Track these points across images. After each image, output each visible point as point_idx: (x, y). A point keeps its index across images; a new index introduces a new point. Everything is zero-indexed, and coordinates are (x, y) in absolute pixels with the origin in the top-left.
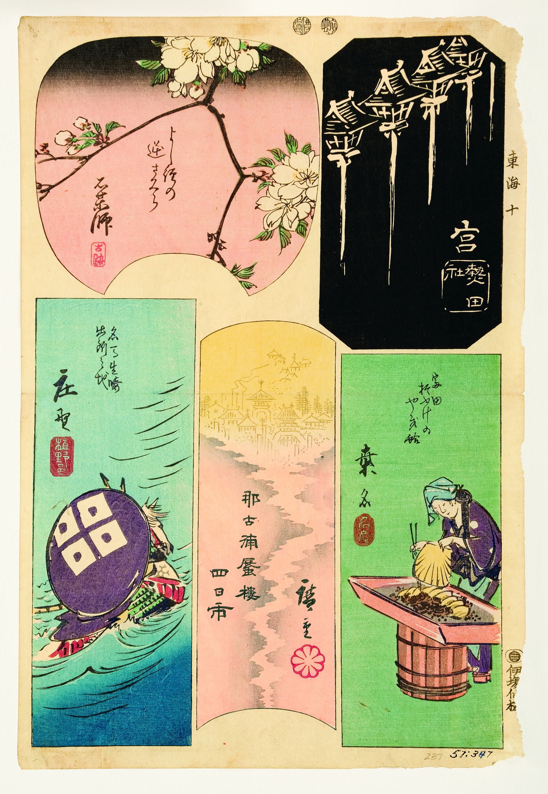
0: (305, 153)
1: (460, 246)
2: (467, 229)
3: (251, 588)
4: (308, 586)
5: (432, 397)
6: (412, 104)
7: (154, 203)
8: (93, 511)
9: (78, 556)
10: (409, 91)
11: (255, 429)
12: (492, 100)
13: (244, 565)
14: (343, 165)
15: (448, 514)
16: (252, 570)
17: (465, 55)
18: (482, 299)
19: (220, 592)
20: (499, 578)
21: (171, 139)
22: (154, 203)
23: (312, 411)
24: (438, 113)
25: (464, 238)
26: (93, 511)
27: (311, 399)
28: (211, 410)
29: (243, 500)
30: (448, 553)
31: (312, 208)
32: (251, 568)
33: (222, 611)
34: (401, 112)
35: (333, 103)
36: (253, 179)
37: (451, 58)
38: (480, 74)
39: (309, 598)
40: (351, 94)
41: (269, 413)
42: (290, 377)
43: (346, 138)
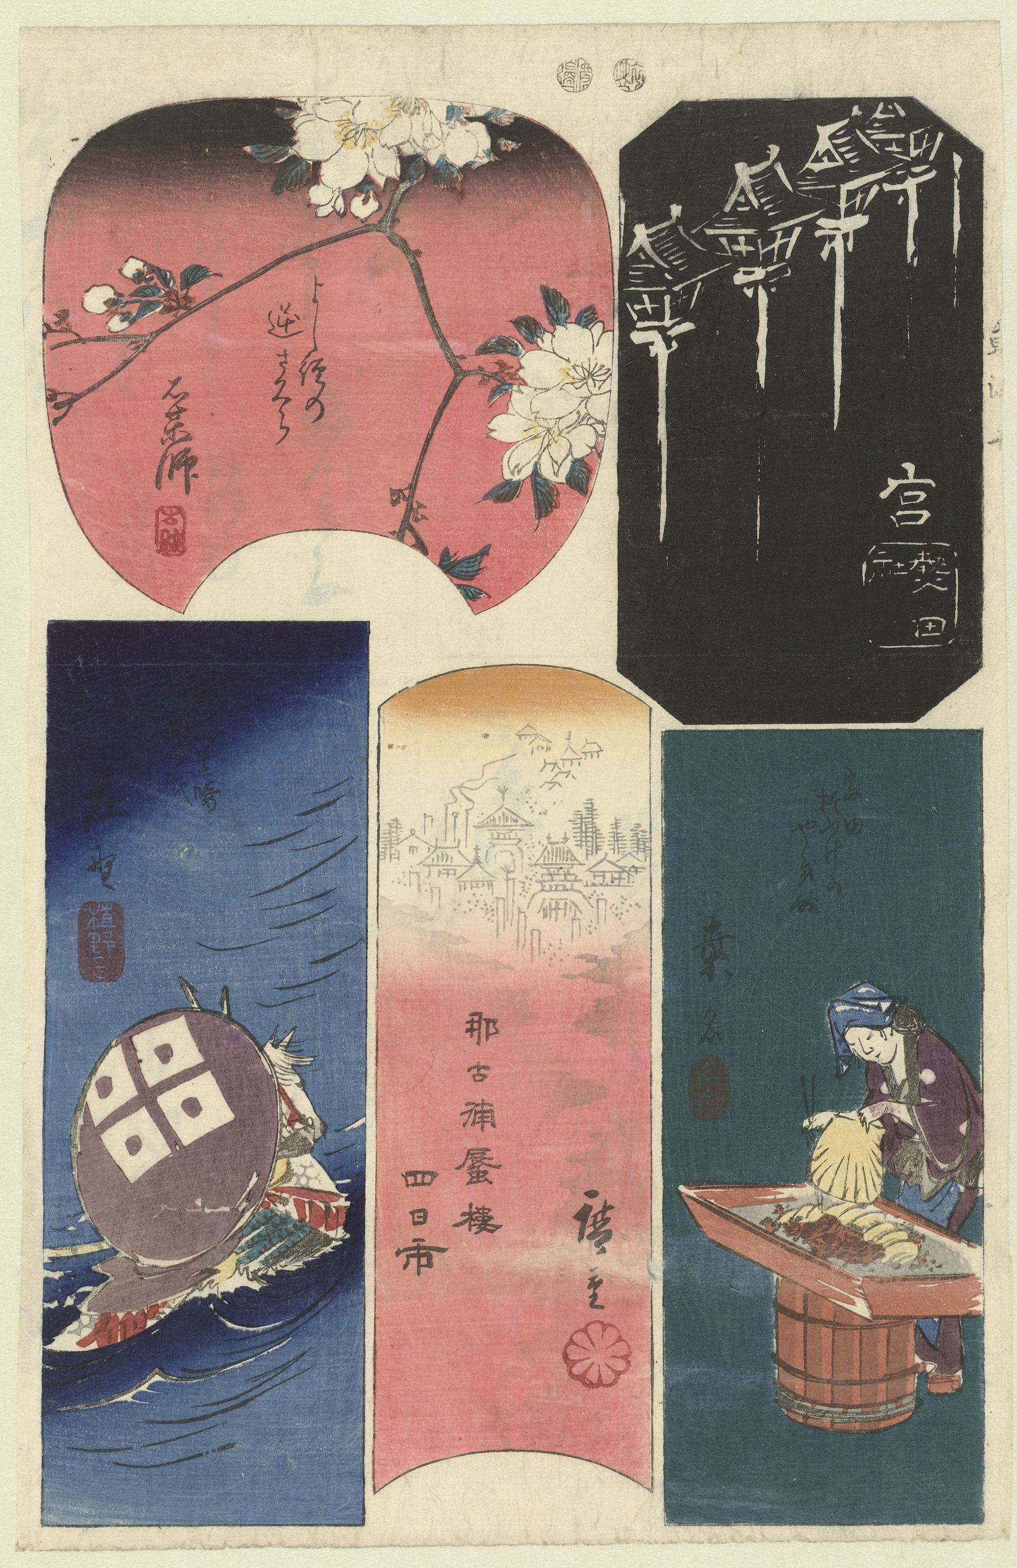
0: (585, 326)
1: (899, 513)
2: (911, 480)
3: (483, 1208)
4: (597, 1205)
5: (845, 820)
6: (798, 230)
7: (282, 427)
8: (165, 1053)
9: (134, 1145)
10: (790, 205)
11: (491, 885)
12: (957, 226)
13: (469, 1162)
14: (660, 351)
15: (878, 1056)
16: (485, 1172)
17: (902, 136)
18: (944, 622)
19: (420, 1217)
20: (980, 1185)
21: (315, 301)
22: (282, 427)
23: (605, 848)
24: (850, 249)
25: (906, 499)
26: (165, 1053)
27: (604, 824)
28: (403, 848)
29: (467, 1031)
30: (877, 1134)
31: (598, 435)
32: (482, 1168)
33: (424, 1255)
34: (776, 245)
35: (641, 231)
36: (479, 378)
37: (874, 142)
38: (932, 174)
39: (600, 1227)
40: (676, 210)
41: (519, 854)
42: (561, 778)
43: (667, 298)
